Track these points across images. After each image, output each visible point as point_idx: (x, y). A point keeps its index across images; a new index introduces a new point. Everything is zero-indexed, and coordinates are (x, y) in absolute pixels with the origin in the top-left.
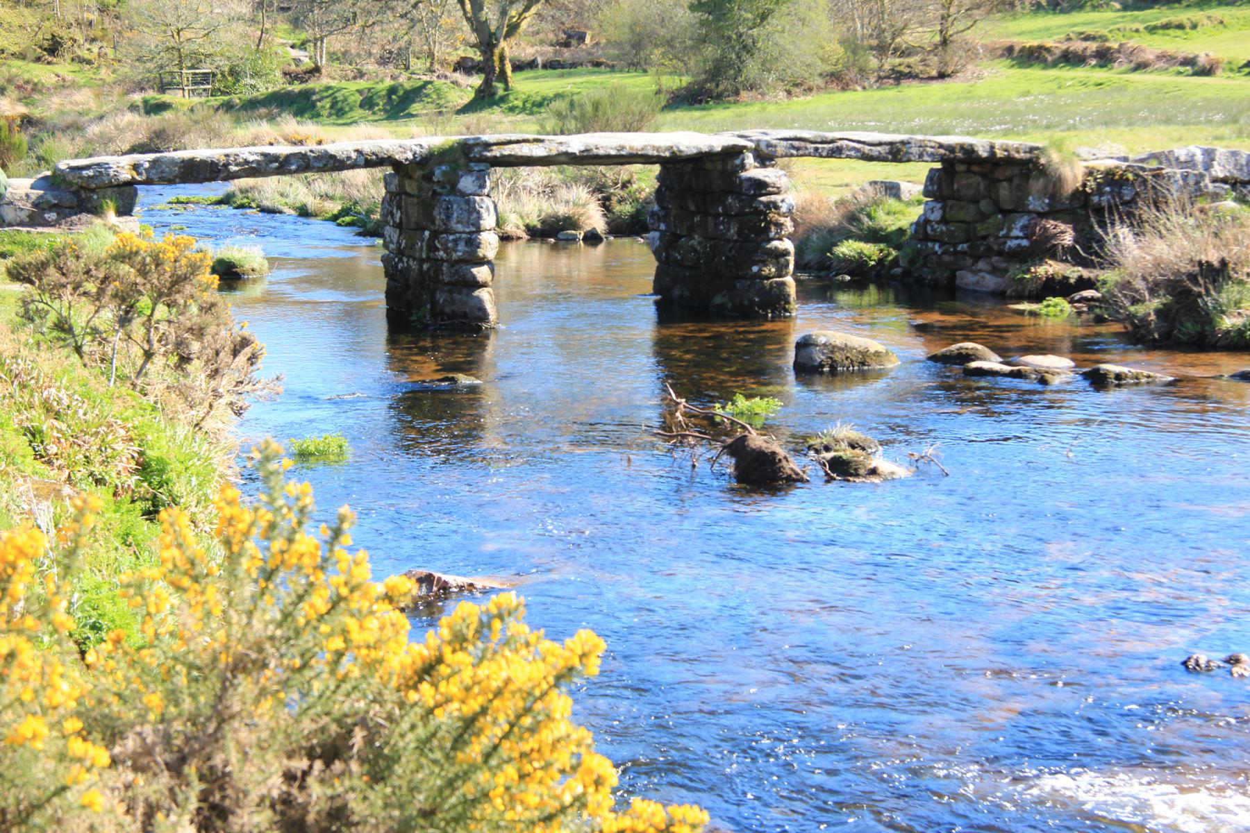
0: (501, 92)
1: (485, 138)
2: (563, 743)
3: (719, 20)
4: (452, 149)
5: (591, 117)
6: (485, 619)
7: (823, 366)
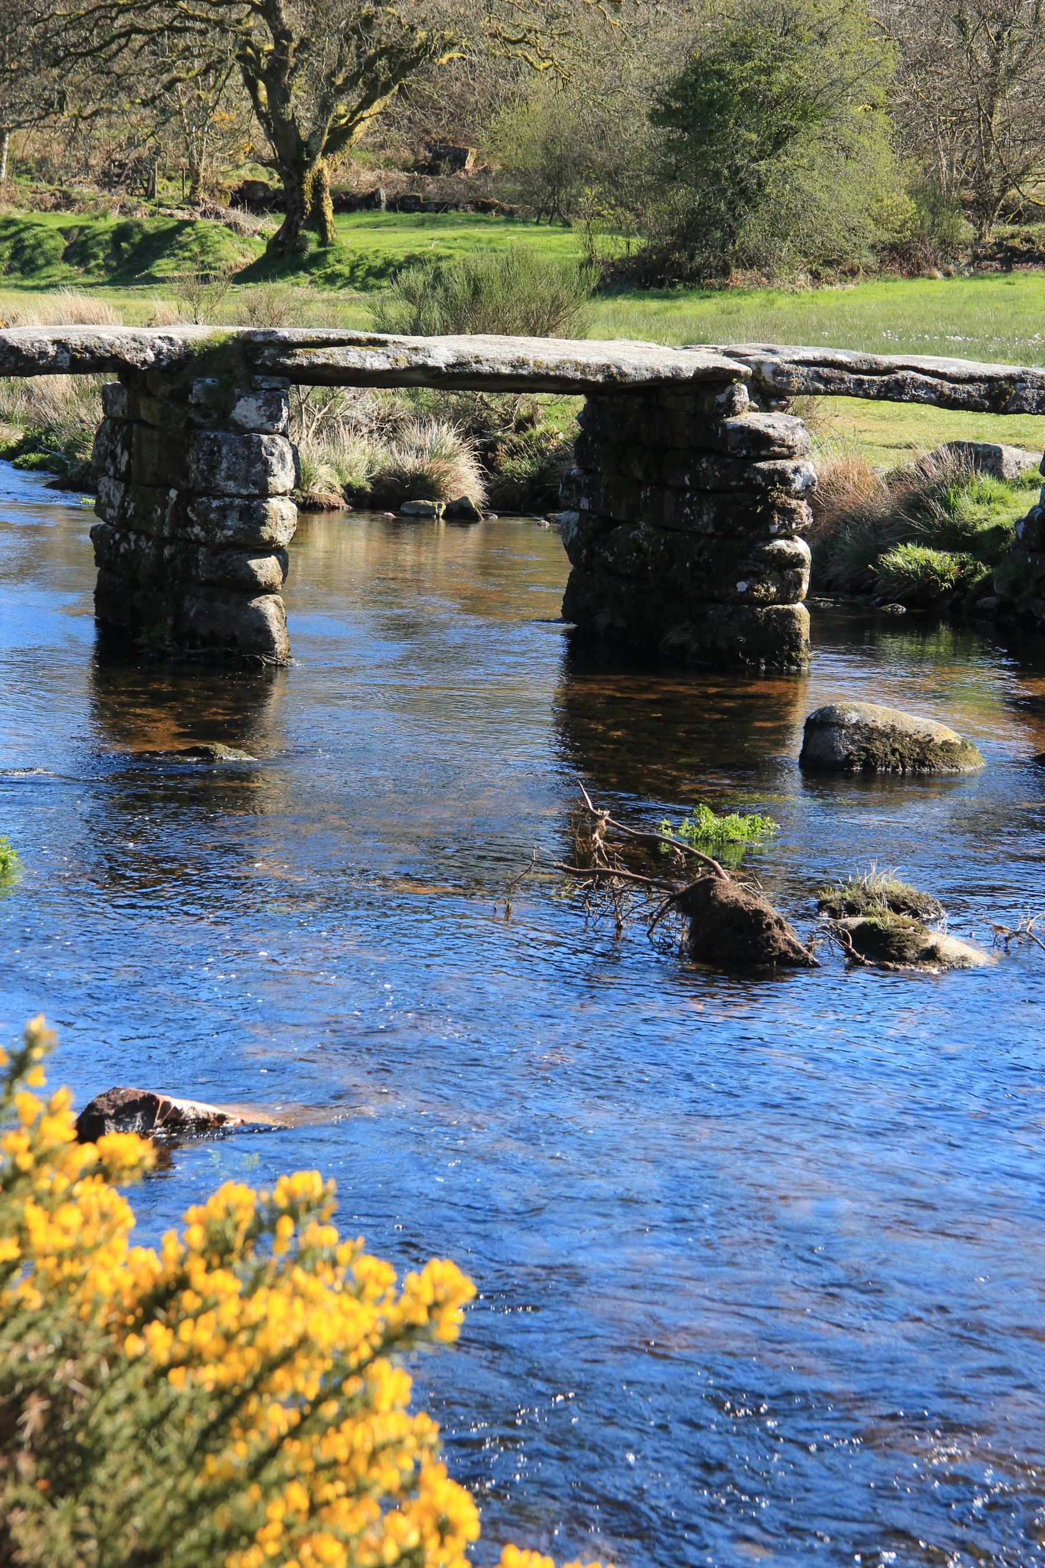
0: (313, 248)
1: (284, 332)
2: (389, 1451)
3: (701, 142)
4: (224, 346)
5: (469, 306)
6: (265, 1215)
7: (852, 763)
